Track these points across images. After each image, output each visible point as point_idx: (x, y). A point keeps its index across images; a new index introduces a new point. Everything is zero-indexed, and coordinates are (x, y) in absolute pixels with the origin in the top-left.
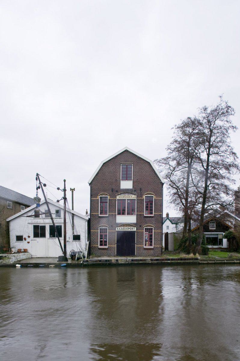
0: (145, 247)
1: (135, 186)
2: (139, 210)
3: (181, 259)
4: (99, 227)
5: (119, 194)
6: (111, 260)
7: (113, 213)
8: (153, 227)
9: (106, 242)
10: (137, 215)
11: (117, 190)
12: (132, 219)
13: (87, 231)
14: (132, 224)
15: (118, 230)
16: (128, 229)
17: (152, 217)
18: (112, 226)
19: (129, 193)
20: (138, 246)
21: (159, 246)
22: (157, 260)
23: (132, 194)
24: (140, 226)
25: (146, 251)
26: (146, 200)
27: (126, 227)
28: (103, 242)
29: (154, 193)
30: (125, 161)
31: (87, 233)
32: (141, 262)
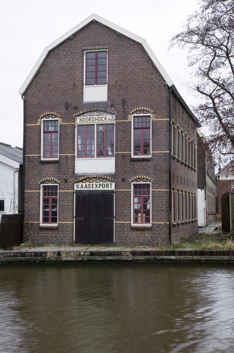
0: (133, 225)
1: (112, 97)
2: (121, 146)
3: (202, 253)
4: (42, 183)
5: (81, 114)
6: (45, 253)
7: (69, 155)
8: (150, 181)
9: (55, 213)
10: (117, 157)
11: (75, 106)
12: (107, 165)
13: (17, 192)
14: (106, 175)
15: (78, 189)
16: (98, 186)
17: (148, 160)
18: (66, 181)
19: (100, 111)
20: (118, 222)
21: (163, 223)
22: (147, 253)
23: (106, 112)
24: (123, 180)
25: (135, 234)
26: (136, 124)
27: (94, 183)
28: (50, 214)
29: (152, 108)
30: (93, 45)
31: (17, 195)
32: (109, 258)
